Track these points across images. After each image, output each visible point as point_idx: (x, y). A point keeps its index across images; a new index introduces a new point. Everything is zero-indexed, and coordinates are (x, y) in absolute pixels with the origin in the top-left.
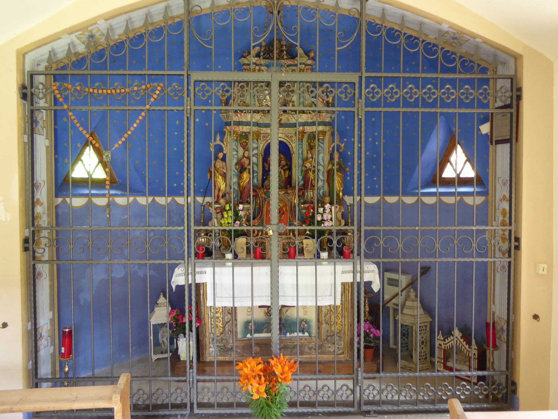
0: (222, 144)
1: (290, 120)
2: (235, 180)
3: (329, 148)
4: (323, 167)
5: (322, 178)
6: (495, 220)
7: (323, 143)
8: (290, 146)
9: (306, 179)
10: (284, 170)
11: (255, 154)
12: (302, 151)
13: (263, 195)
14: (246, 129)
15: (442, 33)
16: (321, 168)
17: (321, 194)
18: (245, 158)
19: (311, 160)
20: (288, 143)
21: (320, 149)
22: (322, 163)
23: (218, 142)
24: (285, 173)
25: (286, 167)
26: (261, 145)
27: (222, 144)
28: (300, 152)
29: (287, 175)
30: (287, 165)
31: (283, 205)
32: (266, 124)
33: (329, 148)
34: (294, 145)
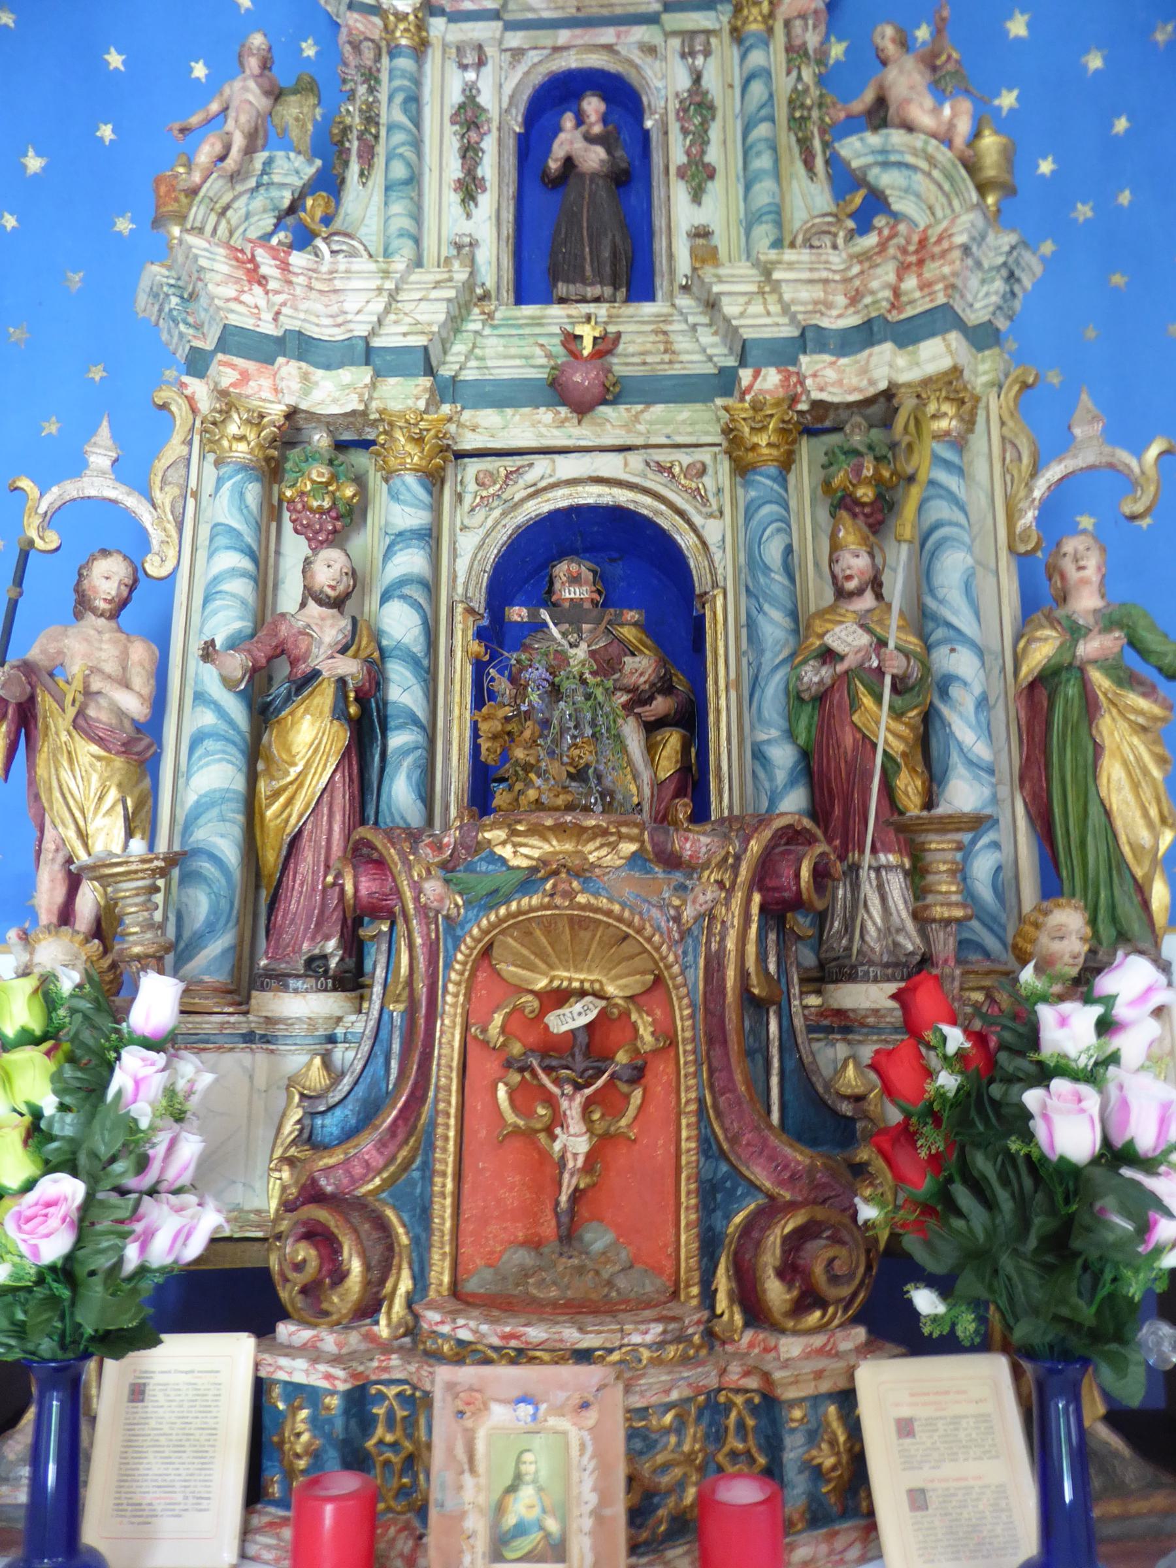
0: (132, 501)
1: (682, 343)
2: (217, 775)
3: (1011, 517)
4: (980, 652)
5: (982, 751)
6: (964, 1392)
7: (960, 471)
8: (686, 541)
9: (830, 778)
10: (651, 728)
11: (403, 582)
12: (789, 550)
13: (433, 888)
14: (333, 393)
15: (880, 1349)
16: (960, 663)
17: (985, 893)
18: (313, 607)
19: (867, 601)
20: (667, 521)
21: (940, 510)
22: (964, 621)
23: (98, 481)
24: (651, 749)
25: (660, 705)
26: (468, 543)
27: (132, 501)
28: (773, 552)
29: (667, 765)
30: (665, 687)
31: (636, 983)
32: (498, 383)
33: (1011, 517)
34: (713, 531)
